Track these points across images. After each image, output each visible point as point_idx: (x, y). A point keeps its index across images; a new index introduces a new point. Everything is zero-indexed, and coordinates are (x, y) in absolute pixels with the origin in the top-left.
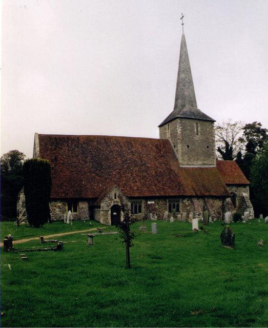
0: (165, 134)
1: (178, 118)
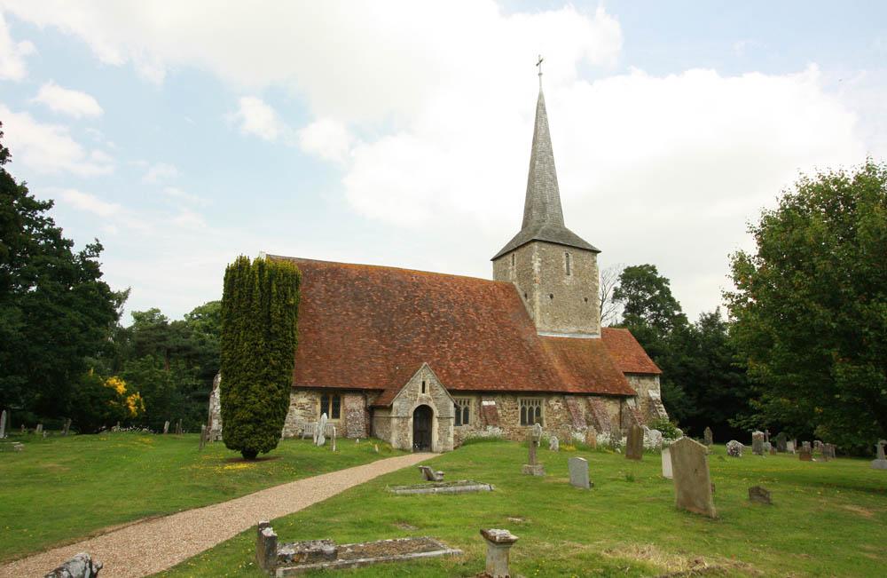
0: (505, 273)
1: (534, 241)
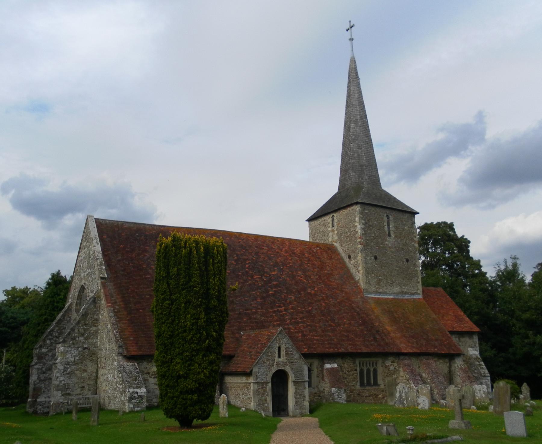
0: (324, 233)
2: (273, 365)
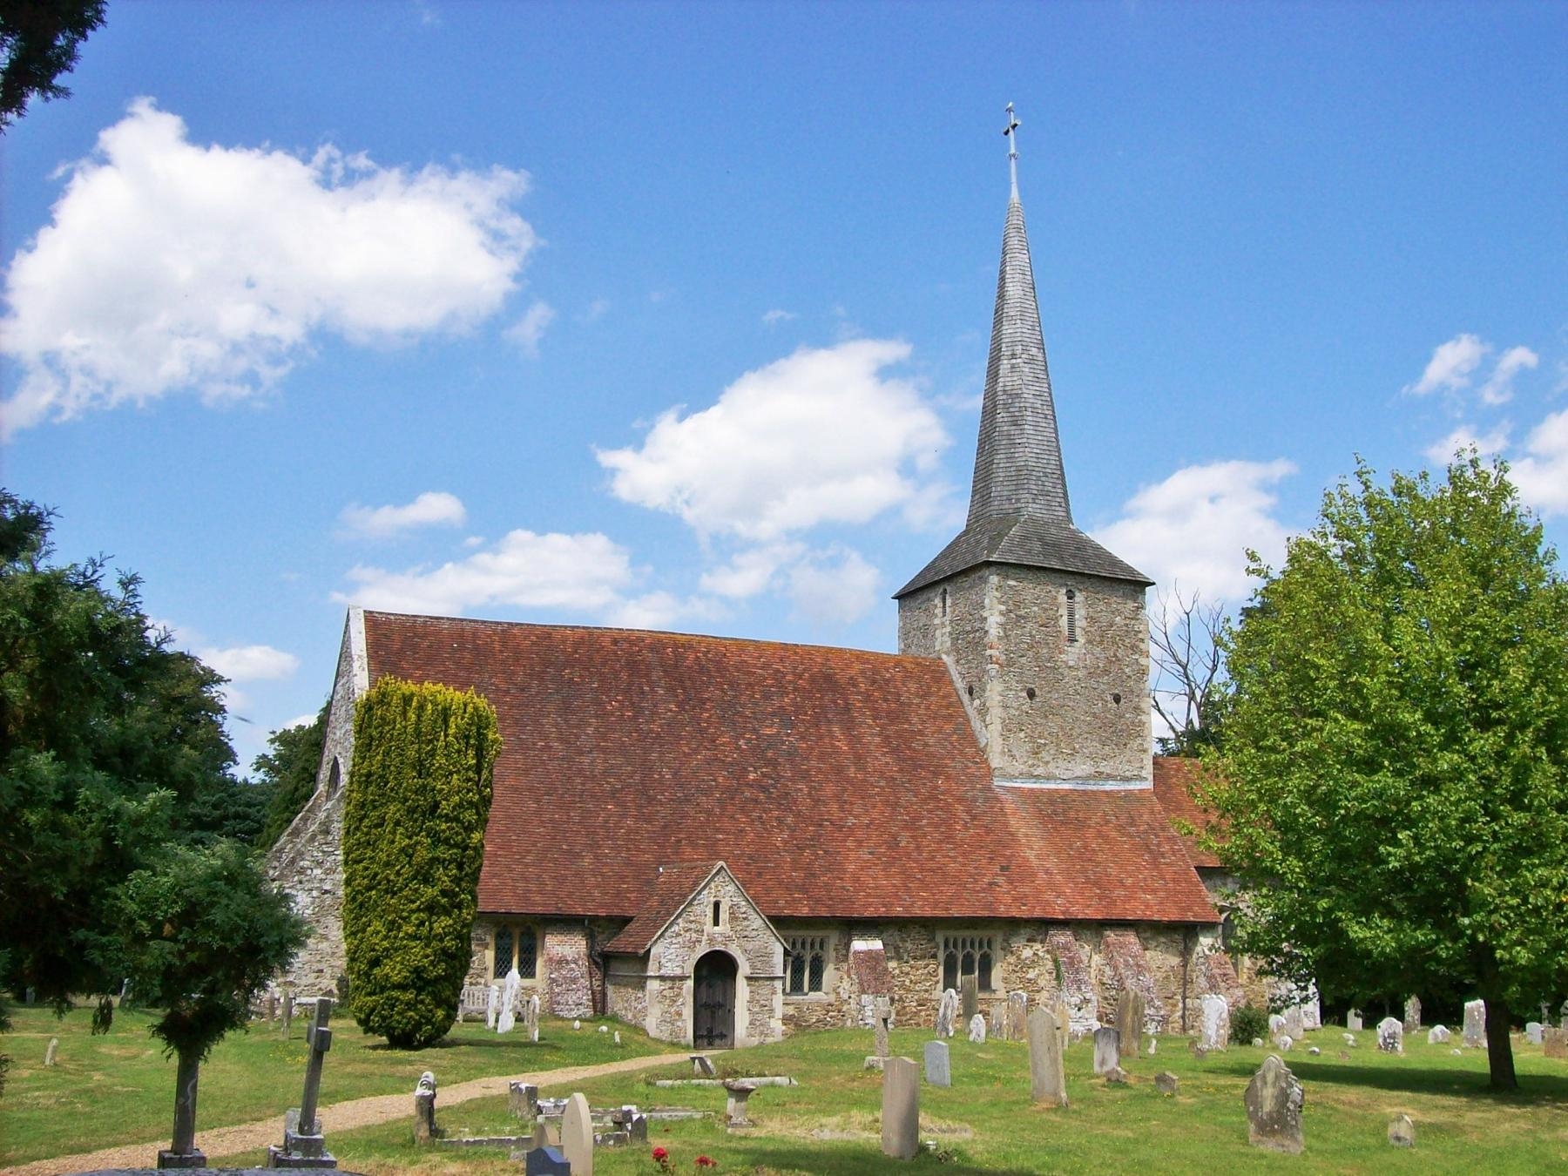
0: (927, 631)
1: (988, 564)
2: (700, 942)
